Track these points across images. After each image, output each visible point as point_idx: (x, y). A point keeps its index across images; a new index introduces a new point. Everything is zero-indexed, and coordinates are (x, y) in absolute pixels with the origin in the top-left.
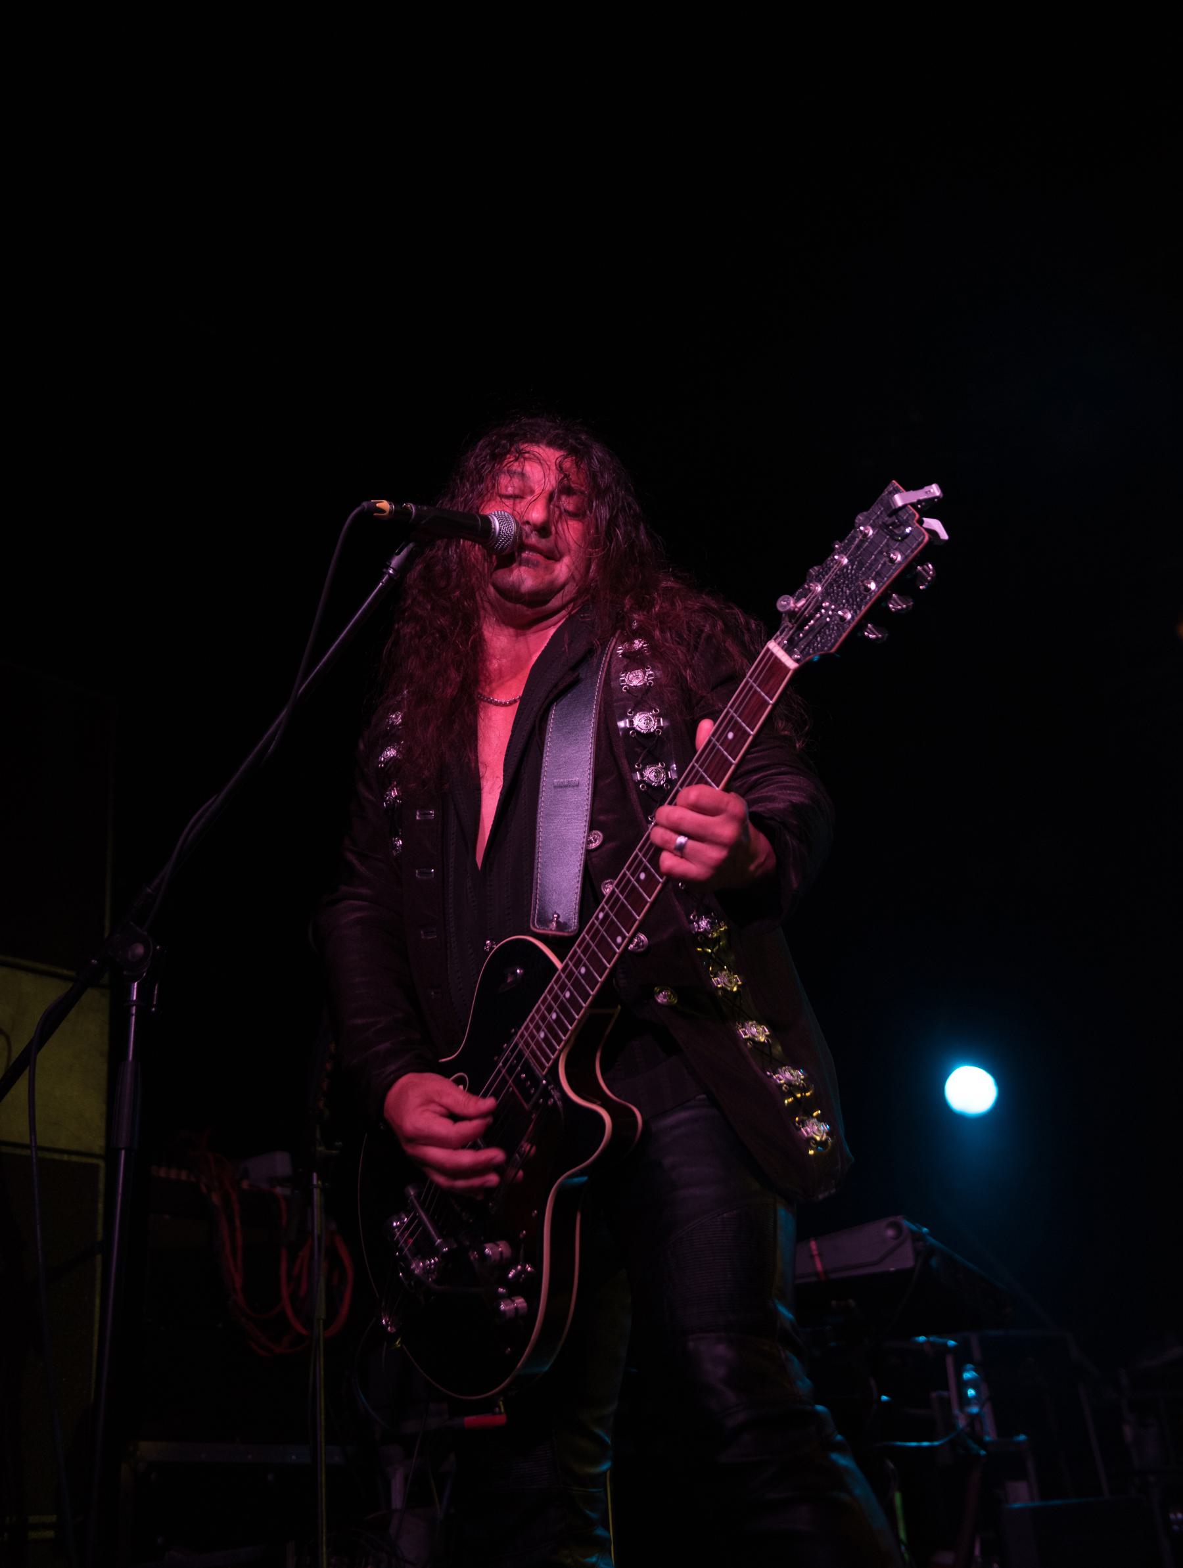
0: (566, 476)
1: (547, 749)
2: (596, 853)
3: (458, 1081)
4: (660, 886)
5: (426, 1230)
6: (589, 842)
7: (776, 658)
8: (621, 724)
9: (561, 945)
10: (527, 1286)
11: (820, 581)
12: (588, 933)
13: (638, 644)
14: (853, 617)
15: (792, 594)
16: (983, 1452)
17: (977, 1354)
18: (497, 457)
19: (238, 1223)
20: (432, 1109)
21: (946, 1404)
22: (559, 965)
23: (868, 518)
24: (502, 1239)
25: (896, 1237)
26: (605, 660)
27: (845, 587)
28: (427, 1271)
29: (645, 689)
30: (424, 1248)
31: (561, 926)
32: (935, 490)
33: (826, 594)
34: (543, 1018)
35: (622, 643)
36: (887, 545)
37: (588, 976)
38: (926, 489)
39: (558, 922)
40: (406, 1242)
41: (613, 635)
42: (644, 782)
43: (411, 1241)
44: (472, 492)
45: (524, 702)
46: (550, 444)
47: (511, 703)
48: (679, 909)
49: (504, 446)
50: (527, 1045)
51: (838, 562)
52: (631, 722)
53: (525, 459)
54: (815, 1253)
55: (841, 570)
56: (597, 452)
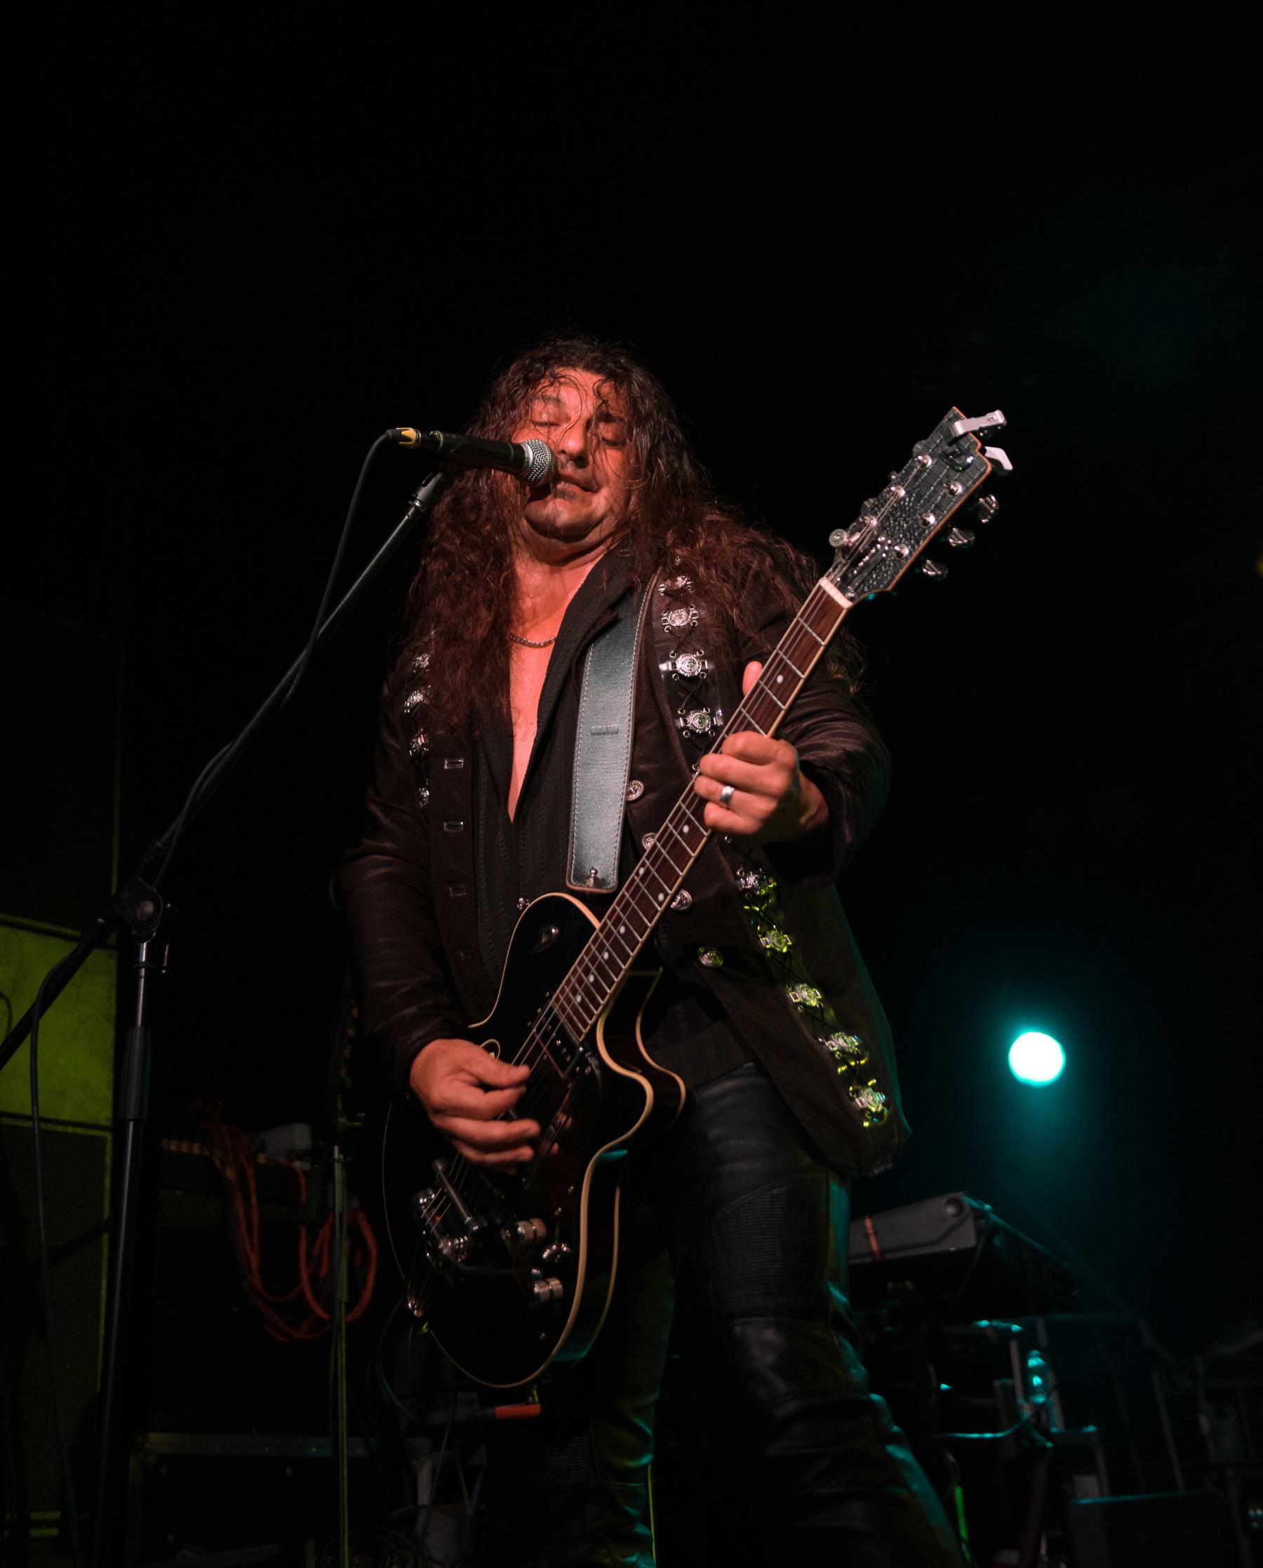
0: (605, 402)
1: (584, 693)
2: (635, 805)
3: (489, 1049)
5: (454, 1206)
6: (629, 793)
7: (829, 596)
8: (663, 667)
9: (599, 903)
10: (563, 1268)
11: (875, 514)
12: (627, 890)
13: (681, 581)
14: (910, 553)
15: (845, 528)
17: (1043, 1339)
18: (531, 382)
19: (254, 1199)
20: (462, 1079)
21: (1010, 1393)
22: (597, 924)
23: (927, 447)
25: (956, 1215)
26: (646, 598)
27: (894, 523)
28: (456, 1251)
29: (689, 630)
30: (453, 1227)
31: (599, 883)
32: (998, 417)
33: (882, 528)
35: (665, 580)
36: (947, 475)
37: (628, 936)
38: (989, 415)
39: (596, 879)
40: (433, 1220)
41: (655, 572)
42: (687, 728)
43: (439, 1219)
44: (504, 418)
46: (587, 368)
47: (545, 645)
49: (538, 369)
51: (895, 494)
52: (674, 665)
54: (870, 1231)
55: (898, 502)
56: (638, 376)
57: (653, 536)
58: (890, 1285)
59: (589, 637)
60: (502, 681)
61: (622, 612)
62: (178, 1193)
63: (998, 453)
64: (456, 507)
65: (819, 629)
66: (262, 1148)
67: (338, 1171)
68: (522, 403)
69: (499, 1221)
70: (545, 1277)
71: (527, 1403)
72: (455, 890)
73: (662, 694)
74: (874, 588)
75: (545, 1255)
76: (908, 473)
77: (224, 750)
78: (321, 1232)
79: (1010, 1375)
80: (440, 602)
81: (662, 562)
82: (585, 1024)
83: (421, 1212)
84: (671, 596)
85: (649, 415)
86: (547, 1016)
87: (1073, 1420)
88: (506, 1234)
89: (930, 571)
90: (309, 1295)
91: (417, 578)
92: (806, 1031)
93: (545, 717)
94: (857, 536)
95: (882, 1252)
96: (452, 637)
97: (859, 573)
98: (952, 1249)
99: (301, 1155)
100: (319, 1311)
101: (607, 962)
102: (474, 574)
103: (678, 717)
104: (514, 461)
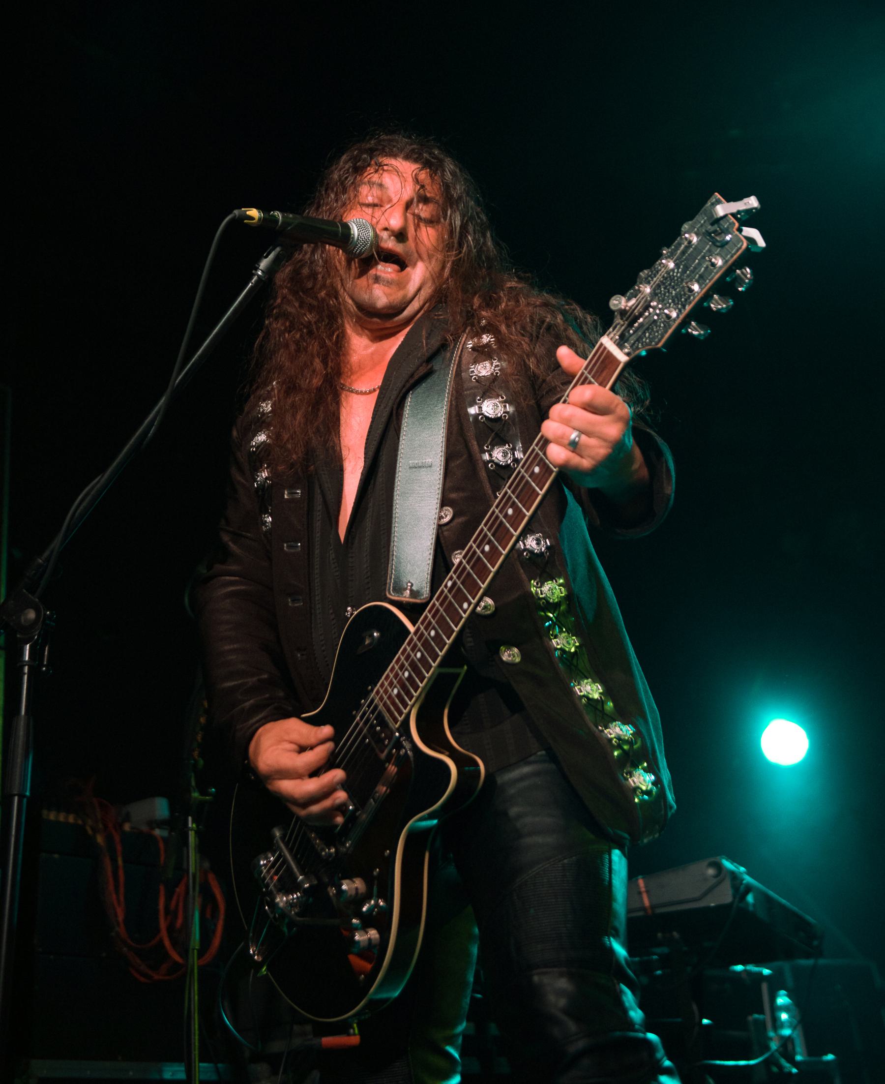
0: (422, 187)
1: (403, 433)
2: (445, 528)
4: (502, 558)
5: (289, 868)
6: (440, 518)
7: (609, 352)
8: (473, 411)
9: (414, 610)
10: (380, 921)
11: (649, 283)
12: (437, 600)
13: (486, 339)
14: (678, 316)
15: (623, 295)
16: (794, 1070)
17: (790, 981)
18: (358, 170)
19: (120, 861)
20: (288, 751)
21: (761, 1027)
22: (412, 629)
23: (693, 227)
24: (357, 876)
25: (716, 876)
26: (457, 354)
27: (669, 290)
28: (291, 905)
29: (494, 378)
30: (288, 885)
31: (414, 594)
32: (753, 202)
33: (654, 294)
34: (396, 676)
35: (472, 338)
36: (709, 251)
37: (438, 639)
38: (746, 200)
39: (411, 590)
40: (272, 878)
41: (464, 331)
42: (493, 461)
43: (276, 878)
44: (337, 201)
45: (384, 390)
46: (407, 158)
47: (370, 392)
48: (524, 577)
49: (365, 160)
50: (381, 699)
51: (665, 266)
52: (480, 408)
53: (384, 170)
54: (643, 889)
55: (668, 273)
56: (449, 165)
57: (463, 301)
58: (659, 935)
59: (408, 385)
60: (333, 424)
61: (437, 364)
62: (56, 856)
63: (753, 233)
64: (296, 278)
65: (601, 379)
66: (127, 818)
67: (192, 837)
68: (352, 188)
69: (326, 880)
70: (365, 926)
71: (349, 1035)
72: (293, 601)
73: (471, 434)
74: (647, 344)
75: (364, 909)
76: (677, 248)
77: (95, 482)
78: (178, 890)
79: (761, 1011)
80: (282, 357)
81: (471, 322)
82: (401, 713)
83: (262, 872)
84: (478, 351)
85: (460, 198)
86: (369, 706)
87: (814, 1048)
88: (333, 891)
89: (695, 331)
90: (167, 943)
91: (261, 336)
92: (589, 718)
93: (371, 454)
94: (633, 302)
95: (653, 907)
96: (291, 387)
97: (635, 332)
98: (713, 905)
99: (161, 824)
100: (176, 957)
101: (419, 660)
102: (310, 333)
103: (484, 451)
104: (343, 238)
